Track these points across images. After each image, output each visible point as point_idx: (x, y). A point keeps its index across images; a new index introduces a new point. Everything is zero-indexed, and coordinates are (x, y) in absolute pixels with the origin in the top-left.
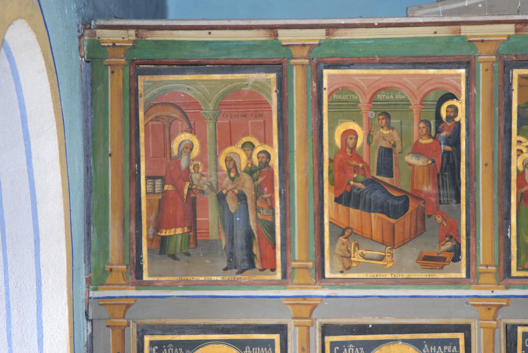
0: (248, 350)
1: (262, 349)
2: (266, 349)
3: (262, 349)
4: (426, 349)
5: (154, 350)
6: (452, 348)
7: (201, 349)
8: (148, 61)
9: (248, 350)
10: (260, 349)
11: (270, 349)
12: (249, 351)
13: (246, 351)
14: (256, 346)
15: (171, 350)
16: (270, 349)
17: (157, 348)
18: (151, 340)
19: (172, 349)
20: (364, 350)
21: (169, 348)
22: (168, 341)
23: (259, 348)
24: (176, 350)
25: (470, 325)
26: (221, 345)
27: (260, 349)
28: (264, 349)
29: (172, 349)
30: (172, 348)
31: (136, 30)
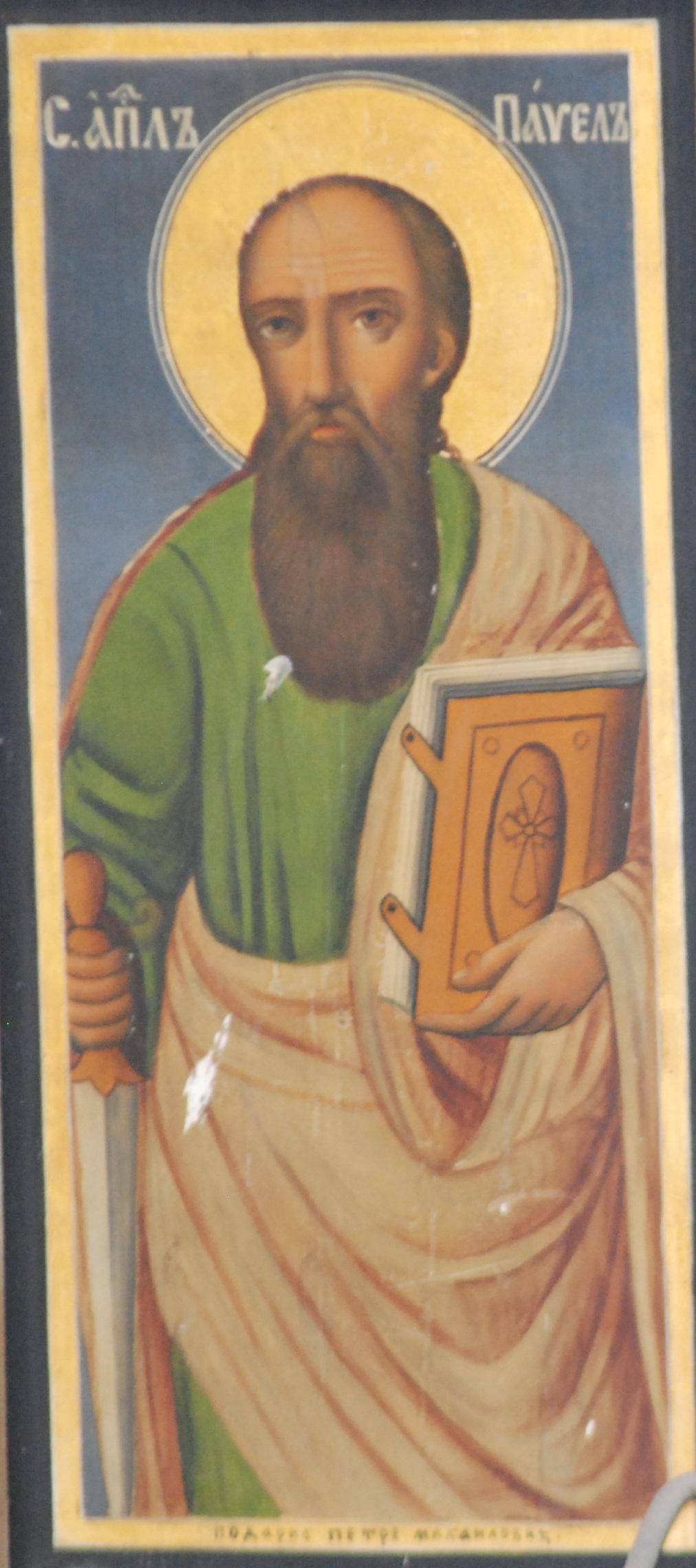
15: (126, 120)
21: (117, 103)
24: (157, 115)
29: (134, 114)
30: (132, 103)
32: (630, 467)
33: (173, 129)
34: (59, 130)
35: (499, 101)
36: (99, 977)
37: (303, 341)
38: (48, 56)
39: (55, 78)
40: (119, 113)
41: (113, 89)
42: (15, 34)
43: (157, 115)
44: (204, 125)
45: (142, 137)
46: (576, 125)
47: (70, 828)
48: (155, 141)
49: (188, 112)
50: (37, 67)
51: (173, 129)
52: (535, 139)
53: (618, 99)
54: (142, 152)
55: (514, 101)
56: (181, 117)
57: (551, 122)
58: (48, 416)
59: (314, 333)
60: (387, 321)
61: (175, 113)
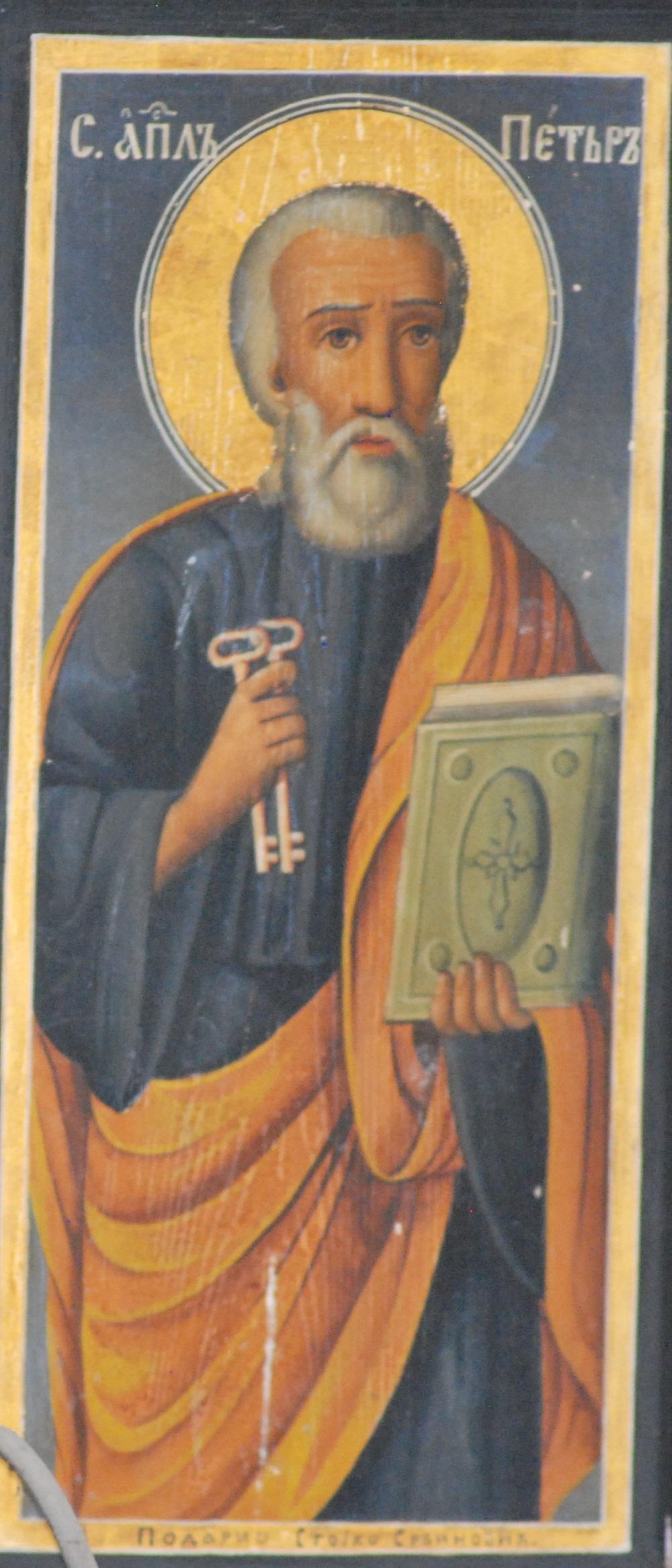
15: (158, 133)
19: (165, 127)
21: (148, 119)
29: (165, 127)
30: (164, 119)
33: (199, 140)
34: (83, 142)
35: (507, 120)
38: (646, 87)
39: (77, 91)
40: (151, 128)
41: (146, 108)
42: (36, 38)
43: (187, 130)
44: (218, 136)
45: (173, 149)
46: (591, 142)
47: (52, 744)
49: (210, 127)
51: (199, 140)
52: (131, 157)
55: (526, 120)
56: (566, 135)
58: (642, 192)
59: (376, 339)
61: (199, 128)
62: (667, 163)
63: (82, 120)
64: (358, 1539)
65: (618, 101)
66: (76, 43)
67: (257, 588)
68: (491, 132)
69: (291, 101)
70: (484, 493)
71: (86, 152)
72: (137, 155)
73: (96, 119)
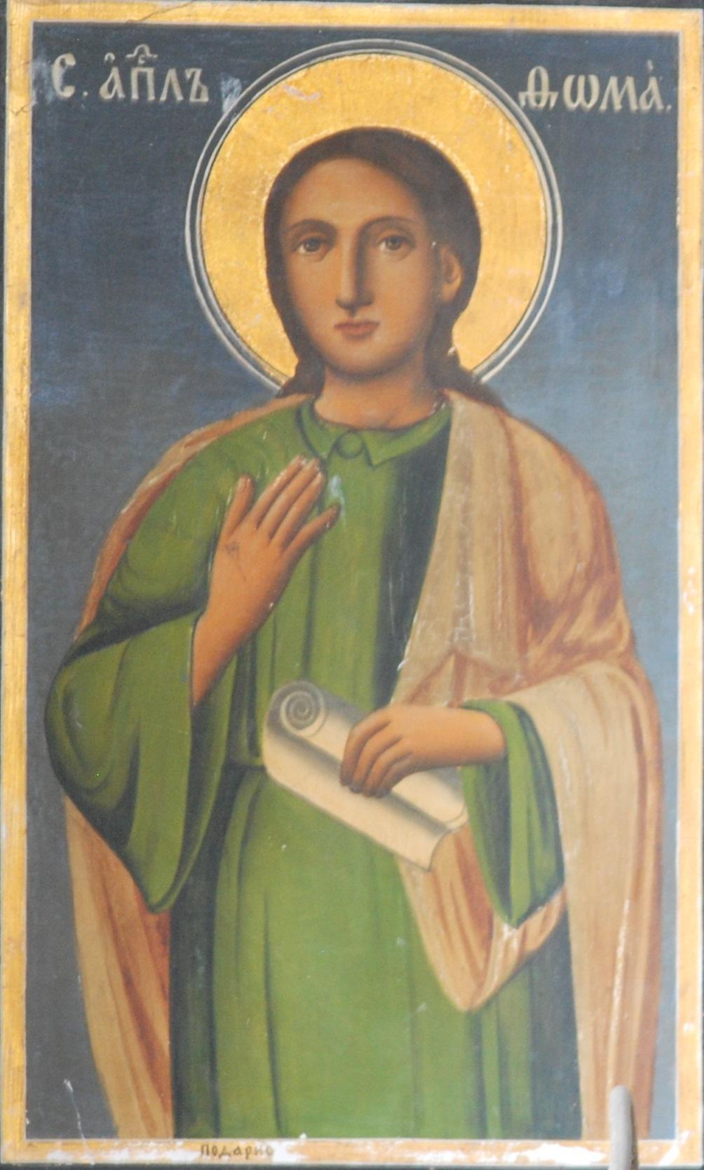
0: (538, 87)
1: (613, 82)
2: (630, 82)
3: (613, 82)
4: (649, 97)
5: (57, 72)
6: (641, 87)
7: (298, 75)
8: (364, 782)
9: (538, 87)
10: (603, 87)
11: (653, 84)
12: (545, 93)
13: (531, 92)
14: (581, 68)
15: (142, 79)
16: (653, 84)
17: (70, 61)
18: (42, 19)
19: (150, 72)
20: (203, 80)
21: (134, 63)
22: (130, 27)
23: (594, 81)
24: (172, 75)
25: (28, 1137)
26: (399, 60)
27: (603, 87)
28: (621, 84)
29: (150, 72)
30: (148, 63)
31: (343, 765)
32: (535, 328)
33: (185, 86)
36: (373, 761)
37: (331, 256)
43: (172, 75)
45: (158, 93)
48: (171, 95)
49: (198, 72)
50: (35, 1141)
51: (185, 86)
53: (246, 79)
54: (156, 103)
57: (586, 94)
59: (346, 245)
60: (403, 249)
62: (288, 3)
63: (63, 63)
64: (248, 1151)
65: (659, 56)
66: (392, 1144)
67: (494, 1111)
68: (514, 85)
69: (555, 169)
70: (494, 377)
71: (69, 92)
72: (121, 95)
73: (76, 57)
